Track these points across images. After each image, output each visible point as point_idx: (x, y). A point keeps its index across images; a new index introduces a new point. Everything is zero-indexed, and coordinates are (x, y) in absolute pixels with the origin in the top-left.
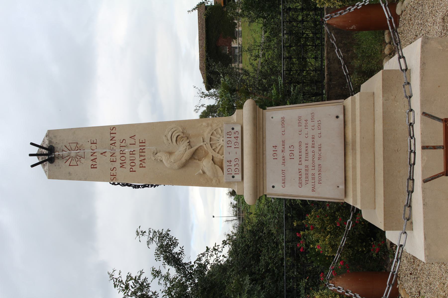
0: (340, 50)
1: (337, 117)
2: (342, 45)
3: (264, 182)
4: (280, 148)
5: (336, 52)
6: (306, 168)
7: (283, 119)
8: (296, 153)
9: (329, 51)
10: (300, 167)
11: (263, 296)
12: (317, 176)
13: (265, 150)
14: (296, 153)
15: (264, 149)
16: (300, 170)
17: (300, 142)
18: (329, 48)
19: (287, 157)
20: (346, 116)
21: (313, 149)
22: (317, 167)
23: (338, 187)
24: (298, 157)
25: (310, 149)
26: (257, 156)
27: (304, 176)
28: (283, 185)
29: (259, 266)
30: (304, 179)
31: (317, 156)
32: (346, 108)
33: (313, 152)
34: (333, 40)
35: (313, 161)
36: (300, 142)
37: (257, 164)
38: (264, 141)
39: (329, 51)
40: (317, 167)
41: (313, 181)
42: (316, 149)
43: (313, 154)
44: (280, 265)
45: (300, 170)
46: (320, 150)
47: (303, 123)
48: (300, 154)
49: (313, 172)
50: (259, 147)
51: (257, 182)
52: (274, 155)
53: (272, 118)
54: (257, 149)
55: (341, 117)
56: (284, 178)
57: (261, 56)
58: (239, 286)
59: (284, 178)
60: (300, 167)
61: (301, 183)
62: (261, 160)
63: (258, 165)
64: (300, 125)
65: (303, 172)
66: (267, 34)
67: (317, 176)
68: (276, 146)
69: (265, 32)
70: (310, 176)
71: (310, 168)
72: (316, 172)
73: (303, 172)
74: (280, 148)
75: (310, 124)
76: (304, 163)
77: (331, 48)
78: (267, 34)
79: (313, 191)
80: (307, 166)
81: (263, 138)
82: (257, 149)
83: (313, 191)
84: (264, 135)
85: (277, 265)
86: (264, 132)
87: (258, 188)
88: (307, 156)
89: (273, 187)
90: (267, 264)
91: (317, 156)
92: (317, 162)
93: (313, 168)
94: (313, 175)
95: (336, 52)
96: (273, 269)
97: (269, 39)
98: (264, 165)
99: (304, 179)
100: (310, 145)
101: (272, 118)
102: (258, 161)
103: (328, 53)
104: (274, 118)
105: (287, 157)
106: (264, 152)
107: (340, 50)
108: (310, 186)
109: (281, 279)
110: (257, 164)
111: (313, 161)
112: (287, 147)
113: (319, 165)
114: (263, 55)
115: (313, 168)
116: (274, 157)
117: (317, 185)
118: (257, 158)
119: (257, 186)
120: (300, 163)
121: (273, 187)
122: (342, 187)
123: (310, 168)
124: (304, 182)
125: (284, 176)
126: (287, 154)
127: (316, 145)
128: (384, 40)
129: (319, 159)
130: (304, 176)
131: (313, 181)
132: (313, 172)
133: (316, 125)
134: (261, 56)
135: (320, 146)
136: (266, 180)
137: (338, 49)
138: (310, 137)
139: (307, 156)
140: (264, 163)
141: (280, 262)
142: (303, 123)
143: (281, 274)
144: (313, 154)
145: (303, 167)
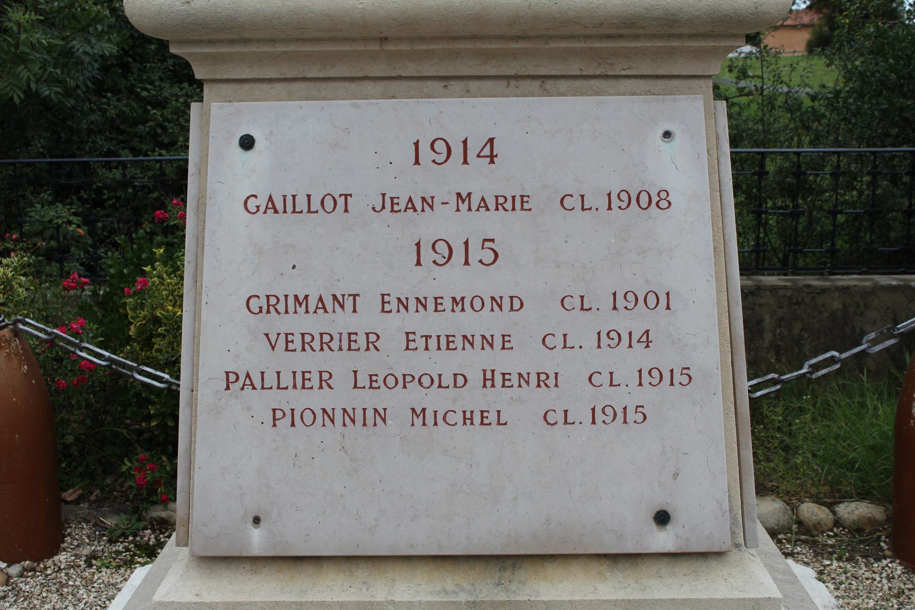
0: (837, 366)
1: (662, 518)
2: (796, 331)
3: (279, 87)
4: (480, 180)
5: (828, 355)
6: (362, 341)
7: (659, 200)
8: (454, 280)
9: (781, 292)
10: (369, 303)
11: (47, 93)
12: (318, 399)
13: (468, 93)
14: (454, 280)
15: (473, 85)
16: (349, 303)
17: (516, 304)
18: (789, 293)
19: (429, 226)
20: (664, 567)
21: (475, 378)
22: (370, 399)
23: (257, 520)
24: (429, 292)
25: (473, 362)
26: (435, 39)
27: (313, 324)
28: (262, 201)
29: (161, 79)
30: (299, 323)
31: (435, 400)
32: (713, 563)
33: (460, 380)
34: (875, 342)
35: (405, 380)
36: (516, 304)
37: (384, 40)
38: (525, 84)
39: (781, 292)
40: (370, 399)
41: (287, 380)
42: (474, 398)
43: (447, 380)
44: (160, 139)
45: (349, 303)
46: (467, 419)
47: (632, 322)
48: (447, 304)
49: (342, 380)
50: (487, 56)
51: (273, 41)
52: (440, 146)
53: (667, 135)
54: (474, 37)
55: (663, 540)
56: (302, 204)
57: (742, 84)
58: (84, 23)
59: (302, 204)
60: (369, 303)
61: (271, 305)
62: (410, 69)
63: (375, 47)
64: (621, 303)
65: (341, 322)
66: (808, 103)
67: (318, 399)
68: (492, 158)
69: (813, 98)
70: (313, 361)
71: (366, 363)
72: (339, 397)
73: (341, 322)
74: (480, 180)
75: (627, 362)
76: (392, 327)
77: (790, 298)
78: (808, 103)
79: (230, 379)
80: (372, 342)
81: (545, 82)
82: (474, 37)
83: (230, 379)
84: (563, 85)
85: (159, 131)
86: (578, 83)
87: (238, 49)
88: (433, 343)
89: (247, 143)
90: (160, 104)
91: (435, 400)
92: (398, 401)
93: (363, 380)
94: (325, 380)
95: (828, 355)
96: (147, 121)
97: (793, 106)
98: (380, 86)
99: (299, 323)
100: (500, 361)
101: (667, 135)
102: (405, 47)
103: (774, 289)
104: (666, 147)
105: (429, 226)
106: (457, 86)
107: (837, 366)
108: (256, 358)
109: (123, 142)
110: (384, 40)
111: (405, 380)
112: (491, 223)
113: (381, 415)
114: (743, 89)
115: (363, 380)
116: (424, 148)
117: (262, 402)
118: (422, 39)
119: (246, 41)
120: (394, 305)
121: (247, 143)
122: (257, 541)
123: (366, 363)
124: (280, 324)
125: (316, 205)
126: (446, 224)
127: (497, 399)
128: (845, 497)
129: (419, 413)
130: (313, 324)
131: (287, 380)
132: (342, 380)
133: (619, 398)
134: (742, 84)
135: (492, 417)
136: (290, 97)
137: (842, 361)
138: (549, 362)
139: (433, 343)
140: (392, 82)
141: (166, 141)
142: (632, 322)
143: (135, 143)
144: (447, 380)
145: (366, 319)
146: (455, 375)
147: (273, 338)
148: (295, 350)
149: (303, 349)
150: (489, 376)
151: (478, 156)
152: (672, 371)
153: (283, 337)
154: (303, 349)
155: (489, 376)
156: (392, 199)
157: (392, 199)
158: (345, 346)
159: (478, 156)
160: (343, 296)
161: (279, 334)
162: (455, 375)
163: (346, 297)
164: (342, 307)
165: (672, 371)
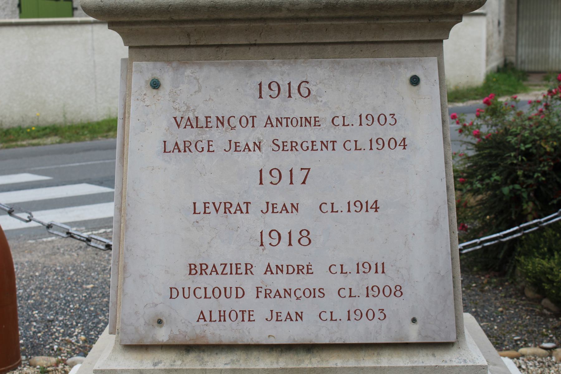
16: (330, 146)
45: (330, 146)
122: (162, 335)
146: (171, 288)
147: (179, 120)
148: (241, 274)
149: (246, 273)
150: (222, 314)
151: (309, 169)
152: (376, 264)
153: (223, 205)
154: (246, 273)
155: (222, 314)
156: (273, 204)
157: (273, 204)
158: (234, 271)
159: (309, 169)
160: (327, 142)
161: (221, 203)
162: (171, 288)
163: (329, 142)
164: (327, 148)
165: (376, 264)
